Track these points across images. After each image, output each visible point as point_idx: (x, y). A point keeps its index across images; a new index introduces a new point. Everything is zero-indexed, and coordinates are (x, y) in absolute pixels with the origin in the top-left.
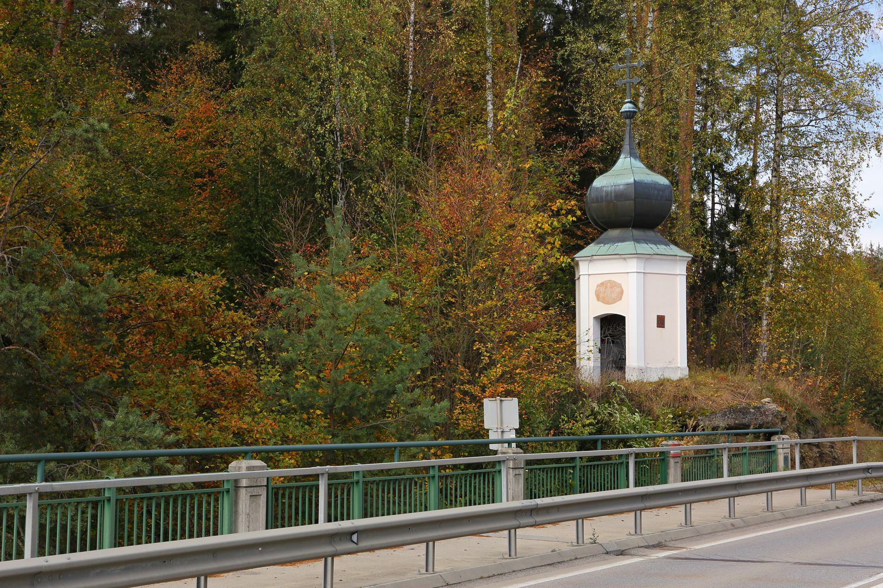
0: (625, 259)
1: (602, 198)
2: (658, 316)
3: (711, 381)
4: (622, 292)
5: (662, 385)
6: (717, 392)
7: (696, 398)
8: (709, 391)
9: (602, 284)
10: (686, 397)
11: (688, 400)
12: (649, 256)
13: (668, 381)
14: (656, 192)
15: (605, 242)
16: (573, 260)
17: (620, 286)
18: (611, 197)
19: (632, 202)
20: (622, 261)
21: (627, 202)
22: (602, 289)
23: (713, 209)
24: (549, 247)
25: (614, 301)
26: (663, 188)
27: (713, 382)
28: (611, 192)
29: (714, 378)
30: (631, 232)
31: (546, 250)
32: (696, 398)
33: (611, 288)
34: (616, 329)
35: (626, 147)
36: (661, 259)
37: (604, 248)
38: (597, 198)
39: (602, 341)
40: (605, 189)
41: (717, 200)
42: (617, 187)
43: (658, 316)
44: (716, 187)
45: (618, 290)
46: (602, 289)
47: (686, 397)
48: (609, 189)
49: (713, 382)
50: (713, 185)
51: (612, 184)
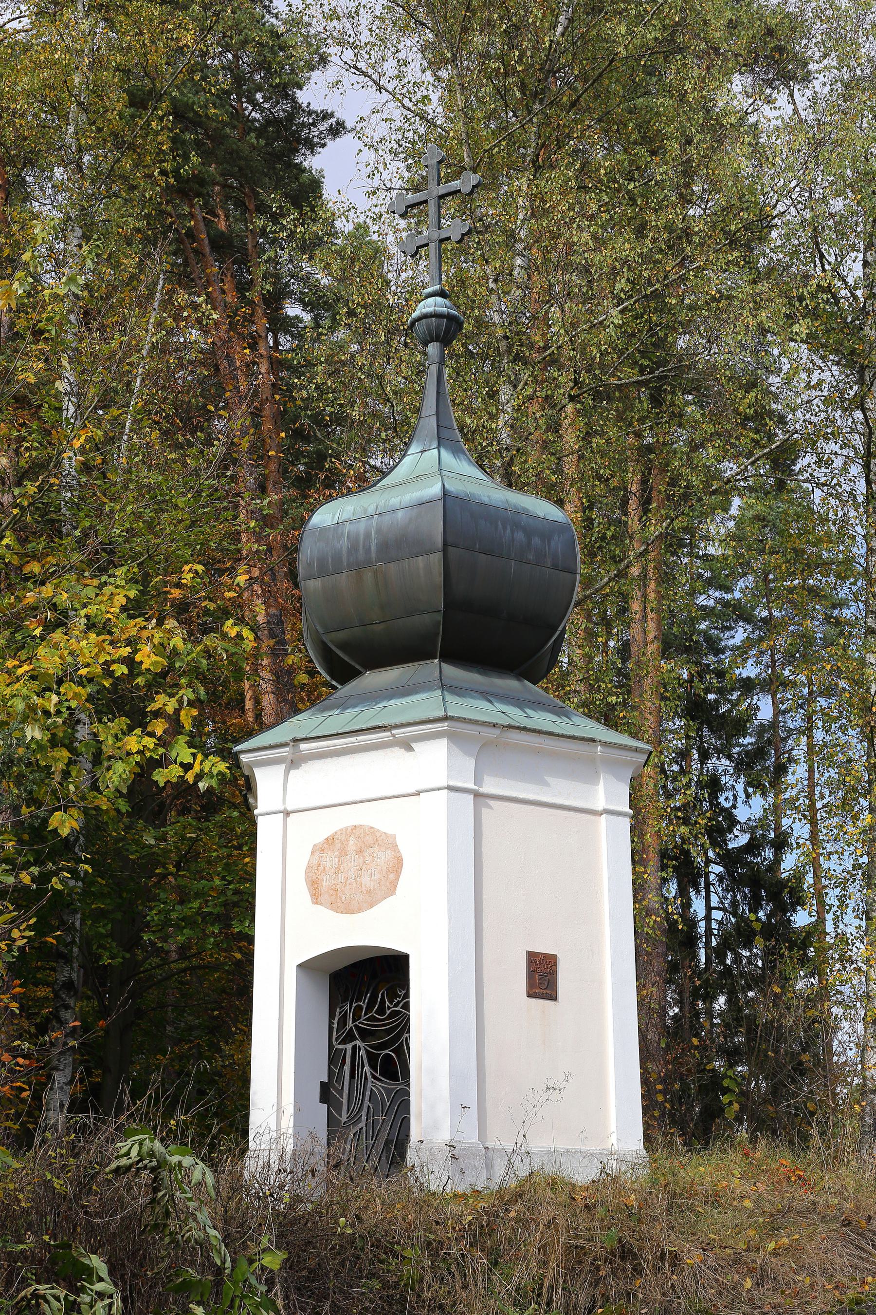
0: (407, 745)
1: (337, 558)
2: (532, 958)
3: (738, 1185)
4: (397, 865)
5: (518, 1196)
6: (772, 1229)
7: (675, 1258)
8: (738, 1228)
9: (330, 841)
10: (626, 1252)
11: (637, 1270)
12: (494, 733)
13: (553, 1184)
14: (520, 536)
15: (343, 706)
16: (235, 763)
17: (390, 843)
18: (368, 550)
19: (436, 559)
20: (398, 753)
21: (420, 561)
22: (330, 860)
23: (708, 918)
24: (159, 727)
25: (371, 900)
26: (551, 529)
27: (748, 1188)
28: (368, 536)
29: (751, 1173)
30: (432, 667)
31: (150, 742)
32: (675, 1258)
33: (360, 851)
34: (381, 1011)
35: (428, 423)
36: (538, 752)
37: (337, 720)
38: (322, 562)
39: (334, 1058)
40: (348, 527)
41: (714, 900)
42: (387, 518)
43: (532, 958)
44: (712, 877)
45: (384, 858)
46: (330, 860)
47: (626, 1252)
48: (362, 526)
49: (748, 1188)
50: (707, 875)
51: (371, 510)
